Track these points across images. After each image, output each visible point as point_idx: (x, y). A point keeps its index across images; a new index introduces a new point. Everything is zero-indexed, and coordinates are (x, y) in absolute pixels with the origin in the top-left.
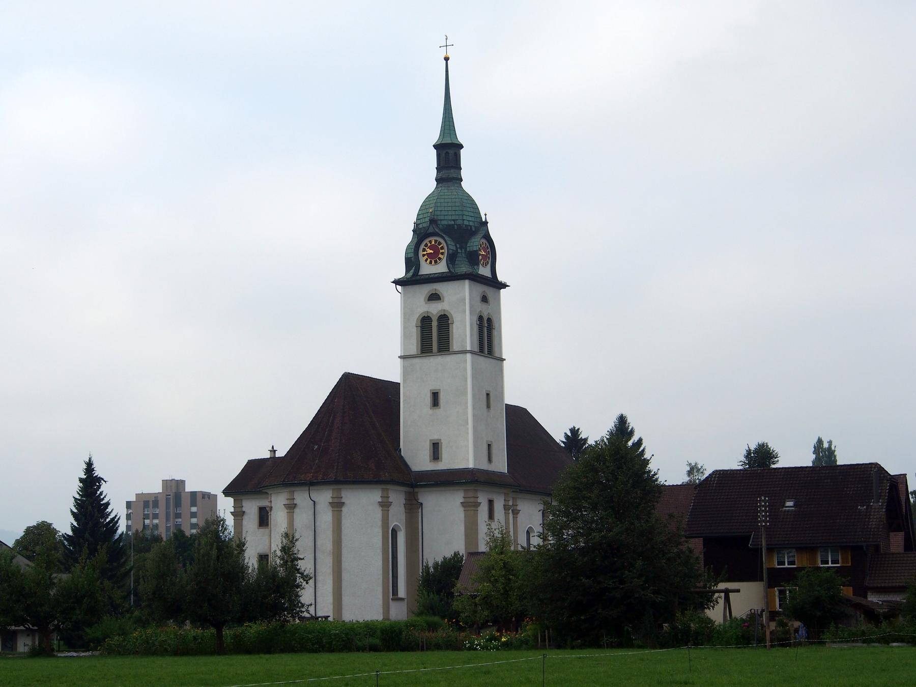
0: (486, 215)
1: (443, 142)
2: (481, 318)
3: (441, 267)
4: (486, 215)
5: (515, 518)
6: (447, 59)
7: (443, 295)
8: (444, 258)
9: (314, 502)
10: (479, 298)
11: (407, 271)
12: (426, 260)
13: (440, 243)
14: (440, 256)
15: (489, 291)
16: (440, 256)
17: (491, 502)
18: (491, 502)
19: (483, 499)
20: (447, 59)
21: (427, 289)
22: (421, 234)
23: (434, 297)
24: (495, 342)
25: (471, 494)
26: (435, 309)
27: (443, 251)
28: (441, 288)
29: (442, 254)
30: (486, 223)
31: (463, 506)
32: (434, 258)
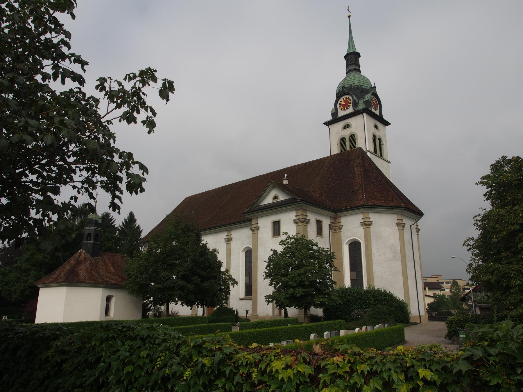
0: (374, 83)
1: (350, 52)
2: (374, 136)
3: (350, 110)
4: (374, 83)
5: (339, 210)
6: (349, 17)
7: (351, 124)
8: (351, 105)
9: (411, 226)
10: (373, 126)
11: (332, 118)
12: (342, 109)
13: (349, 98)
14: (349, 104)
15: (380, 125)
16: (349, 104)
17: (319, 223)
18: (319, 223)
19: (312, 218)
20: (349, 17)
21: (342, 124)
22: (339, 95)
23: (347, 126)
24: (382, 150)
25: (300, 212)
26: (347, 133)
27: (350, 102)
28: (350, 121)
29: (350, 103)
30: (375, 87)
31: (398, 226)
32: (345, 106)
